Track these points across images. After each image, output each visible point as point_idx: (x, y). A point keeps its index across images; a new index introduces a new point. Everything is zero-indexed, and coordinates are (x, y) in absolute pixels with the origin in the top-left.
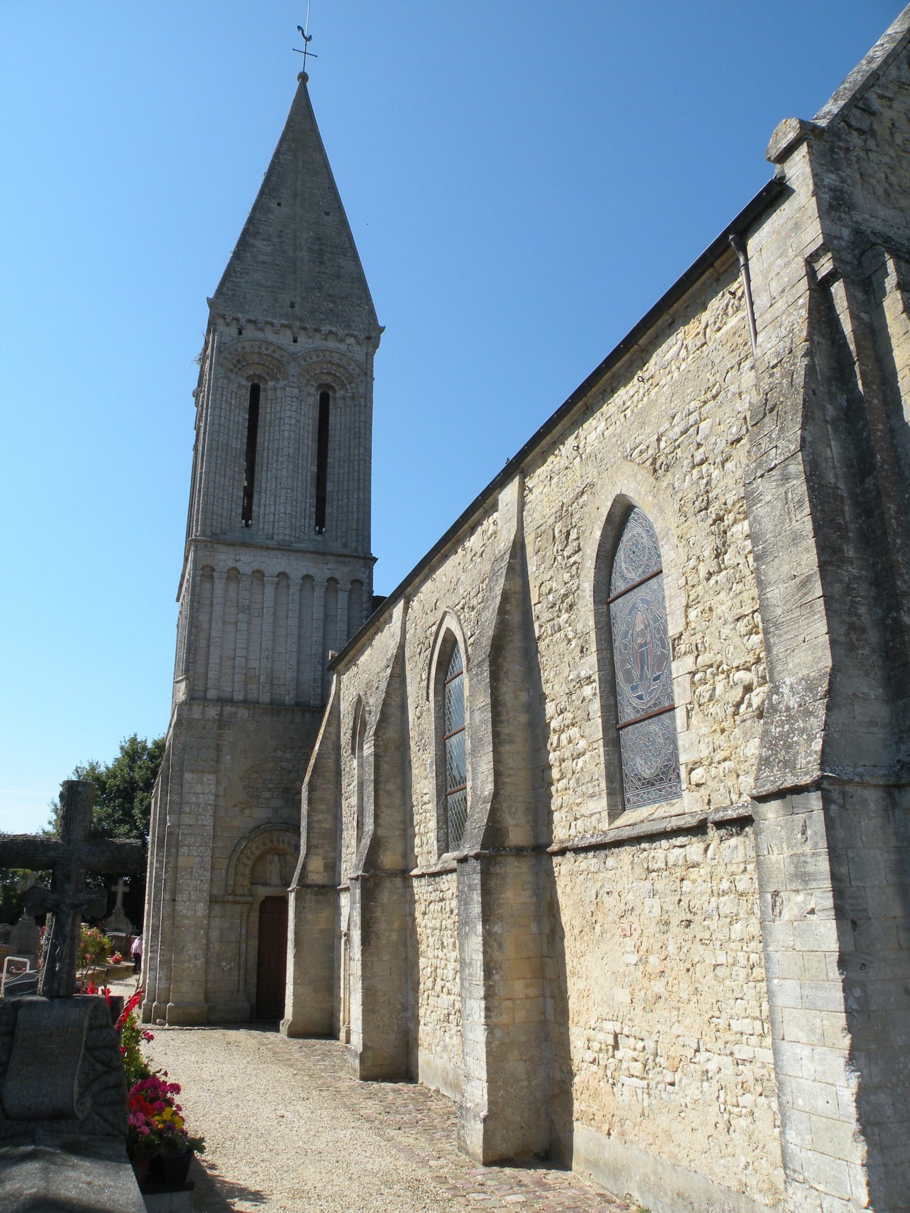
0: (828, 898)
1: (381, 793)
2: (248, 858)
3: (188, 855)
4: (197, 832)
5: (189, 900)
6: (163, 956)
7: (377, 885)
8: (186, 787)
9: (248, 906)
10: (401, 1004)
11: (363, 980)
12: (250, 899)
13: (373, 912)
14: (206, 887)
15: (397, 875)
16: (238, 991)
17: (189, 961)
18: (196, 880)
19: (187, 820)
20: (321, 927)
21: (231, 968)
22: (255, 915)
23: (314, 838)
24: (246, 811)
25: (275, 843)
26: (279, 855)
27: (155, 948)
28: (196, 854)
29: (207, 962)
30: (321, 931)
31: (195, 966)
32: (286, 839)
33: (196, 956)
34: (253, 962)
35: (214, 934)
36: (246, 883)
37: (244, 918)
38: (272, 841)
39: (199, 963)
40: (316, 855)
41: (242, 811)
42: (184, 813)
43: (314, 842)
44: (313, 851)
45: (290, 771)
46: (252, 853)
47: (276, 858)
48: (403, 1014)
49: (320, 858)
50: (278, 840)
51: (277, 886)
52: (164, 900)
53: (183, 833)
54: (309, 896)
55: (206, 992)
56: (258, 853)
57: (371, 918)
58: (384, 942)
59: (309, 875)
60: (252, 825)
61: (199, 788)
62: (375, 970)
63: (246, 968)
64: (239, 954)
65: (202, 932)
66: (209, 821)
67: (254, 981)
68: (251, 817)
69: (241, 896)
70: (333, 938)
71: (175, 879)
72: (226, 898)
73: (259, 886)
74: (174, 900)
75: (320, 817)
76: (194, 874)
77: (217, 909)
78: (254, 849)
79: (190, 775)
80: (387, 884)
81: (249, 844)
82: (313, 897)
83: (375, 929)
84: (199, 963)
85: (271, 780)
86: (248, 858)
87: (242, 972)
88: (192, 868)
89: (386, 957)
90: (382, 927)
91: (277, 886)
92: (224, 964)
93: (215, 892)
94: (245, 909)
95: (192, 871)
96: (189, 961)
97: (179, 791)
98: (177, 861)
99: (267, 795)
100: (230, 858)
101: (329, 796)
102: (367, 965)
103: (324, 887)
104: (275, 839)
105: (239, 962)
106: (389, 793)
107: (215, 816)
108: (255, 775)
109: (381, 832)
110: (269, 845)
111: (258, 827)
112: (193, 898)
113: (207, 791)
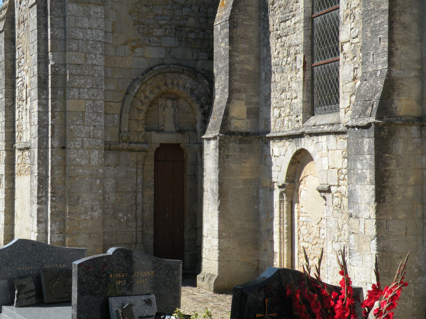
0: (301, 140)
1: (396, 25)
2: (142, 102)
3: (79, 99)
4: (86, 72)
5: (82, 147)
6: (55, 207)
7: (391, 134)
8: (70, 20)
9: (144, 154)
10: (418, 267)
11: (378, 241)
12: (145, 146)
13: (388, 165)
14: (100, 133)
15: (413, 123)
16: (136, 244)
17: (86, 213)
18: (89, 126)
19: (73, 58)
20: (245, 177)
21: (128, 219)
22: (150, 164)
23: (236, 81)
24: (137, 50)
25: (170, 86)
26: (173, 99)
27: (43, 199)
28: (87, 97)
29: (104, 213)
30: (245, 182)
31: (92, 218)
32: (181, 83)
33: (92, 208)
34: (149, 213)
35: (110, 184)
36: (141, 129)
37: (140, 166)
38: (166, 84)
39: (96, 214)
40: (239, 99)
41: (133, 49)
42: (71, 50)
43: (236, 85)
44: (235, 95)
45: (183, 6)
46: (146, 97)
47: (169, 103)
48: (420, 278)
49: (243, 103)
50: (172, 84)
51: (171, 132)
52: (52, 147)
53: (71, 74)
54: (233, 145)
55: (104, 245)
56: (152, 96)
57: (385, 171)
58: (399, 198)
59: (233, 121)
60: (144, 66)
61: (86, 23)
62: (391, 229)
63: (143, 220)
64: (136, 205)
65: (98, 182)
66: (98, 60)
67: (152, 232)
68: (143, 57)
69: (136, 143)
70: (258, 188)
71: (64, 125)
72: (121, 146)
73: (154, 133)
74: (64, 148)
75: (242, 57)
76: (86, 119)
77: (111, 156)
78: (147, 93)
79: (75, 6)
80: (402, 133)
81: (143, 87)
82: (237, 146)
83: (390, 184)
84: (96, 214)
85: (162, 15)
86: (142, 102)
87: (139, 223)
88: (83, 112)
89: (402, 216)
90: (396, 181)
91: (171, 132)
92: (121, 215)
93: (109, 139)
94: (140, 156)
95: (83, 116)
96: (86, 213)
97: (62, 25)
98: (65, 105)
99: (159, 32)
100: (123, 101)
101: (251, 34)
102: (382, 224)
103: (247, 134)
104: (169, 81)
105: (136, 214)
106: (405, 27)
107: (105, 55)
108: (144, 9)
109: (396, 72)
110: (164, 88)
111: (151, 69)
112: (86, 145)
113: (95, 26)
